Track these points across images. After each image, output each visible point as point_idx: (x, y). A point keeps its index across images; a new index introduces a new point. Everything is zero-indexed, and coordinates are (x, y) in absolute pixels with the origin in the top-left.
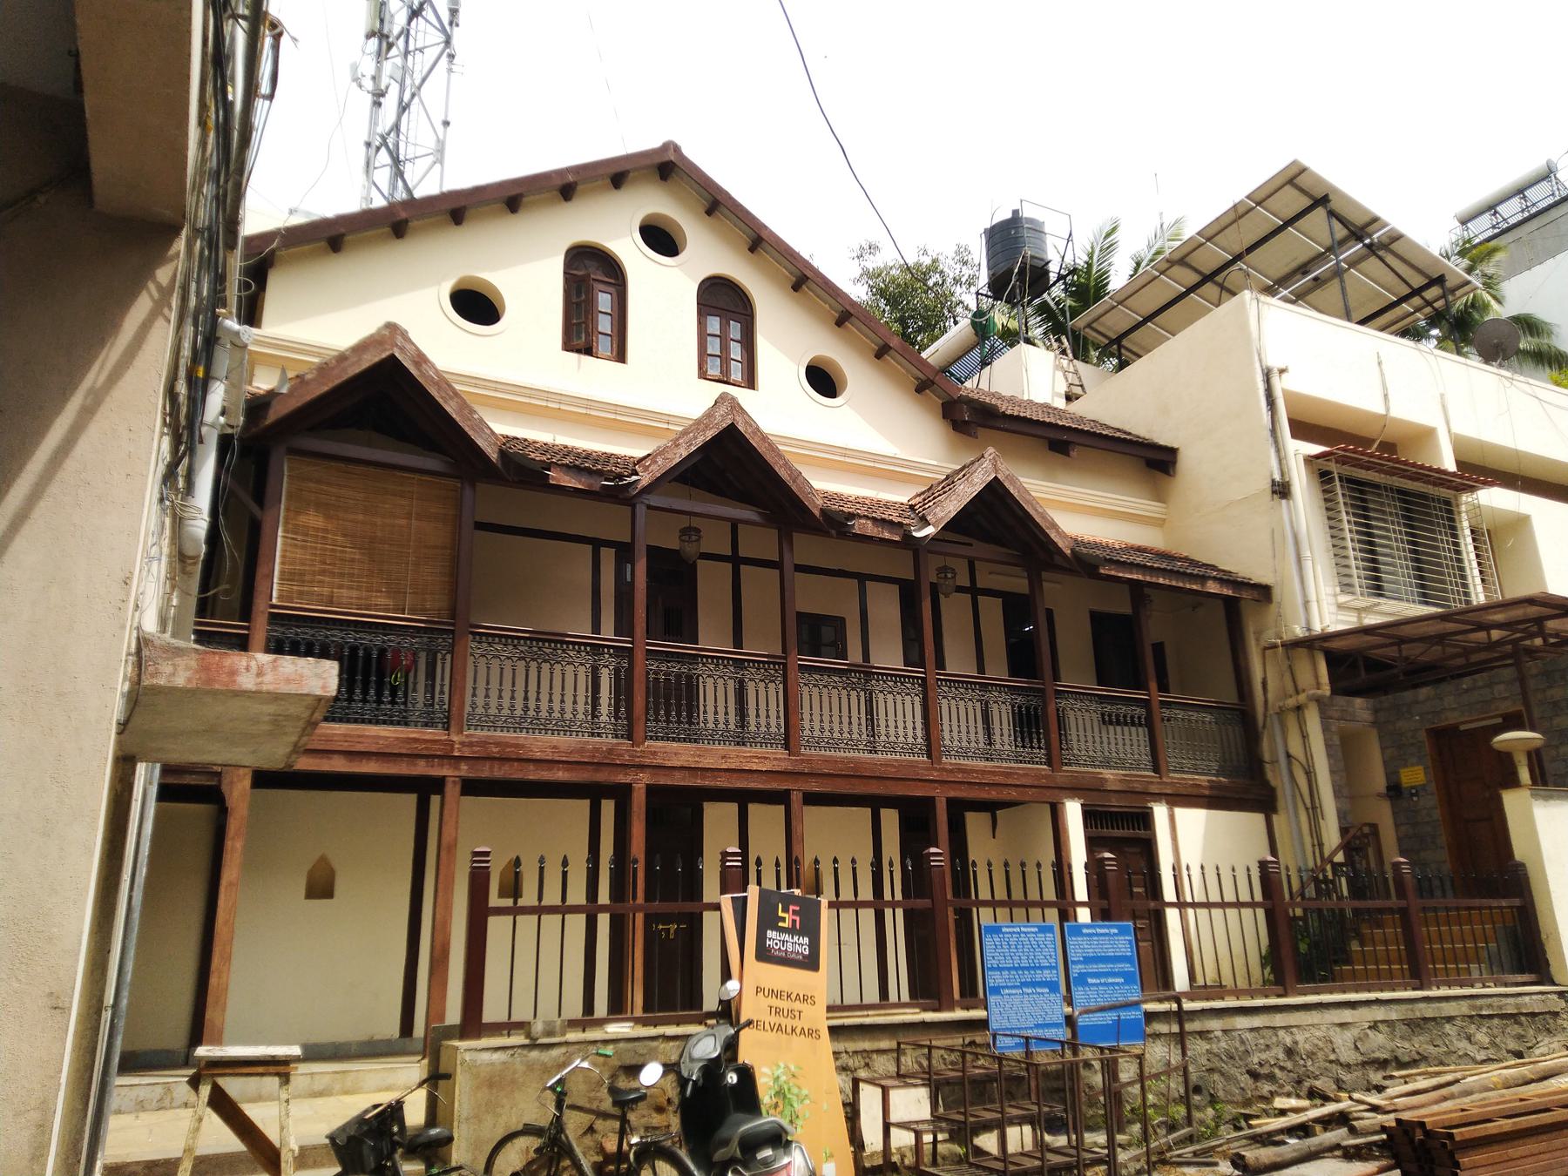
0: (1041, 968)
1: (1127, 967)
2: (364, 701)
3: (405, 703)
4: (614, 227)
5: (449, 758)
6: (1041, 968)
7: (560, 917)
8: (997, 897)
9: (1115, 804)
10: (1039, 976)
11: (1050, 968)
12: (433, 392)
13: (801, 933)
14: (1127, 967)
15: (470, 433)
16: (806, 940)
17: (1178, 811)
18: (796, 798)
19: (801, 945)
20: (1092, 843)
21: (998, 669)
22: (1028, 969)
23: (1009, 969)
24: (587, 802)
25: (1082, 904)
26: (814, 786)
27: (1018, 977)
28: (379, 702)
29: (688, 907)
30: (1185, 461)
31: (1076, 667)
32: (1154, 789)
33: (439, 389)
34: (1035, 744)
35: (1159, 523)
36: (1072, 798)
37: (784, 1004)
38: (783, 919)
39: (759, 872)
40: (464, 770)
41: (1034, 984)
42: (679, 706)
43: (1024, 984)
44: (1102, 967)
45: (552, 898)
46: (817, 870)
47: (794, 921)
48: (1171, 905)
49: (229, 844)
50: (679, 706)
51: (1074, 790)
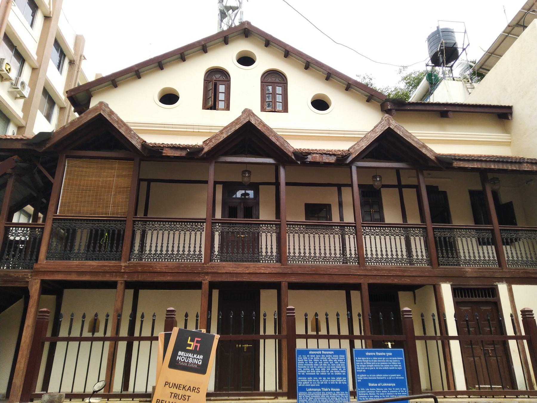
0: (336, 376)
1: (398, 377)
2: (227, 253)
3: (457, 257)
4: (225, 58)
5: (119, 273)
6: (336, 376)
7: (149, 342)
8: (342, 333)
9: (473, 284)
10: (333, 381)
11: (342, 376)
12: (116, 125)
13: (199, 353)
14: (398, 377)
15: (130, 139)
16: (202, 357)
17: (514, 287)
18: (284, 286)
19: (198, 359)
20: (457, 304)
21: (414, 219)
22: (326, 376)
23: (313, 376)
24: (132, 291)
25: (454, 338)
26: (293, 279)
27: (318, 382)
28: (243, 253)
29: (253, 336)
30: (516, 111)
31: (461, 215)
32: (497, 275)
33: (118, 123)
34: (450, 255)
35: (508, 144)
36: (445, 282)
37: (180, 392)
38: (190, 345)
39: (265, 320)
40: (126, 278)
41: (329, 386)
42: (442, 250)
43: (322, 386)
44: (379, 377)
45: (76, 333)
46: (317, 319)
47: (196, 346)
48: (511, 338)
49: (29, 310)
50: (442, 250)
51: (446, 278)
